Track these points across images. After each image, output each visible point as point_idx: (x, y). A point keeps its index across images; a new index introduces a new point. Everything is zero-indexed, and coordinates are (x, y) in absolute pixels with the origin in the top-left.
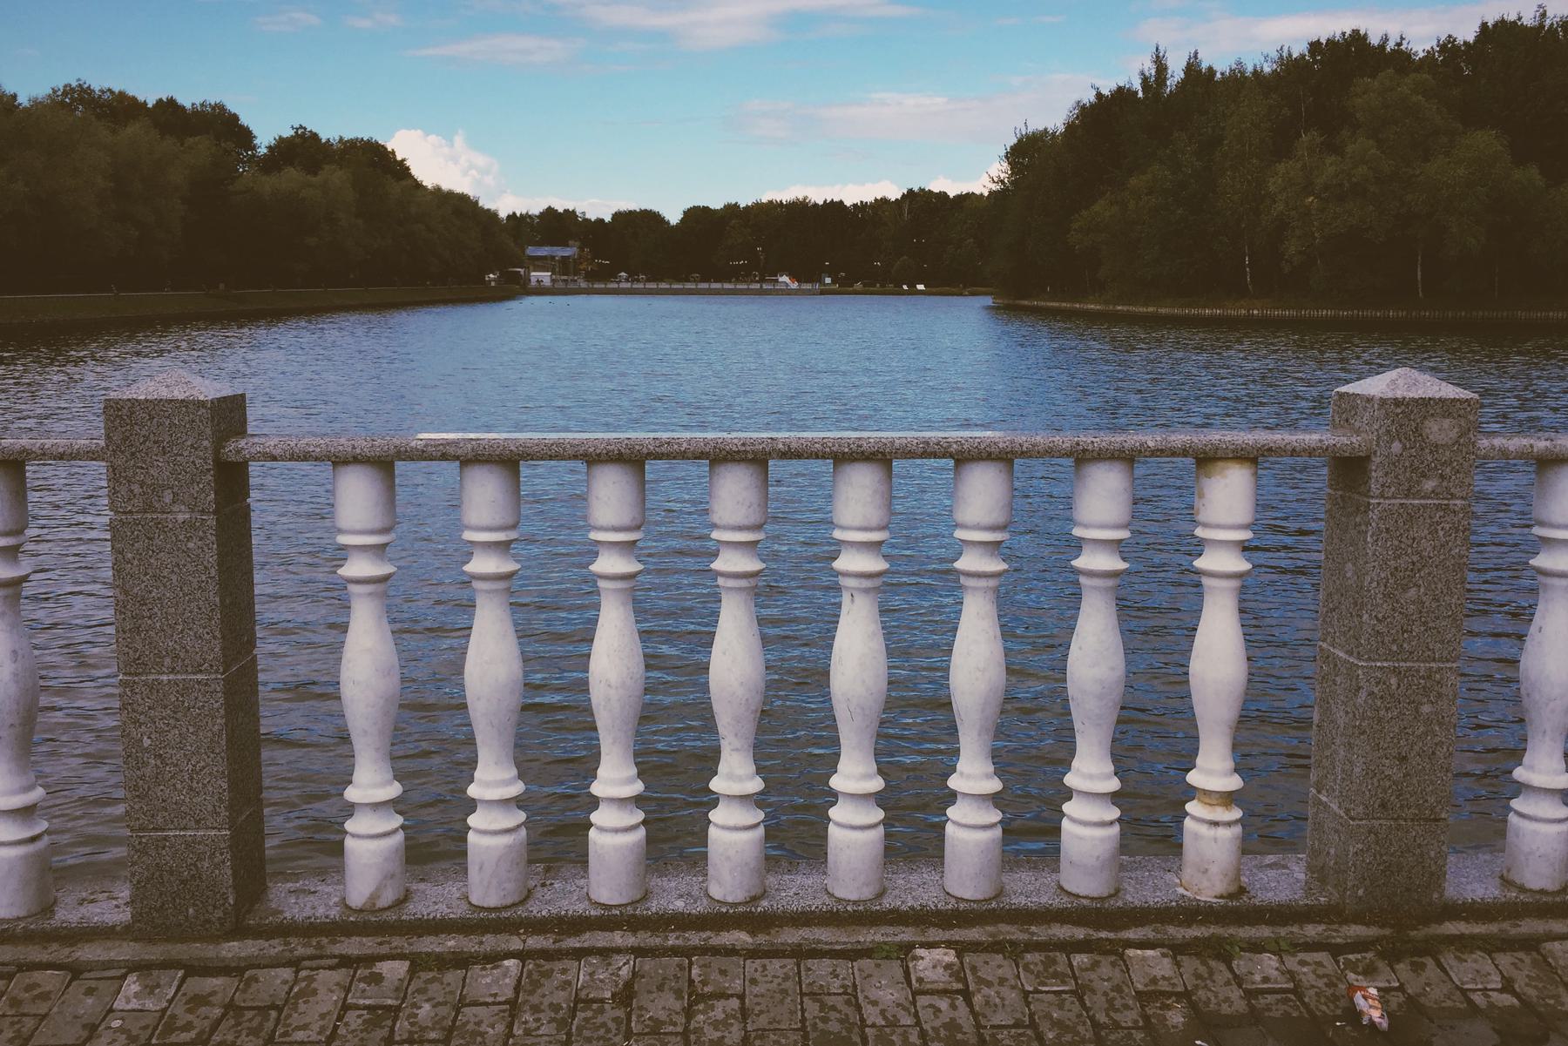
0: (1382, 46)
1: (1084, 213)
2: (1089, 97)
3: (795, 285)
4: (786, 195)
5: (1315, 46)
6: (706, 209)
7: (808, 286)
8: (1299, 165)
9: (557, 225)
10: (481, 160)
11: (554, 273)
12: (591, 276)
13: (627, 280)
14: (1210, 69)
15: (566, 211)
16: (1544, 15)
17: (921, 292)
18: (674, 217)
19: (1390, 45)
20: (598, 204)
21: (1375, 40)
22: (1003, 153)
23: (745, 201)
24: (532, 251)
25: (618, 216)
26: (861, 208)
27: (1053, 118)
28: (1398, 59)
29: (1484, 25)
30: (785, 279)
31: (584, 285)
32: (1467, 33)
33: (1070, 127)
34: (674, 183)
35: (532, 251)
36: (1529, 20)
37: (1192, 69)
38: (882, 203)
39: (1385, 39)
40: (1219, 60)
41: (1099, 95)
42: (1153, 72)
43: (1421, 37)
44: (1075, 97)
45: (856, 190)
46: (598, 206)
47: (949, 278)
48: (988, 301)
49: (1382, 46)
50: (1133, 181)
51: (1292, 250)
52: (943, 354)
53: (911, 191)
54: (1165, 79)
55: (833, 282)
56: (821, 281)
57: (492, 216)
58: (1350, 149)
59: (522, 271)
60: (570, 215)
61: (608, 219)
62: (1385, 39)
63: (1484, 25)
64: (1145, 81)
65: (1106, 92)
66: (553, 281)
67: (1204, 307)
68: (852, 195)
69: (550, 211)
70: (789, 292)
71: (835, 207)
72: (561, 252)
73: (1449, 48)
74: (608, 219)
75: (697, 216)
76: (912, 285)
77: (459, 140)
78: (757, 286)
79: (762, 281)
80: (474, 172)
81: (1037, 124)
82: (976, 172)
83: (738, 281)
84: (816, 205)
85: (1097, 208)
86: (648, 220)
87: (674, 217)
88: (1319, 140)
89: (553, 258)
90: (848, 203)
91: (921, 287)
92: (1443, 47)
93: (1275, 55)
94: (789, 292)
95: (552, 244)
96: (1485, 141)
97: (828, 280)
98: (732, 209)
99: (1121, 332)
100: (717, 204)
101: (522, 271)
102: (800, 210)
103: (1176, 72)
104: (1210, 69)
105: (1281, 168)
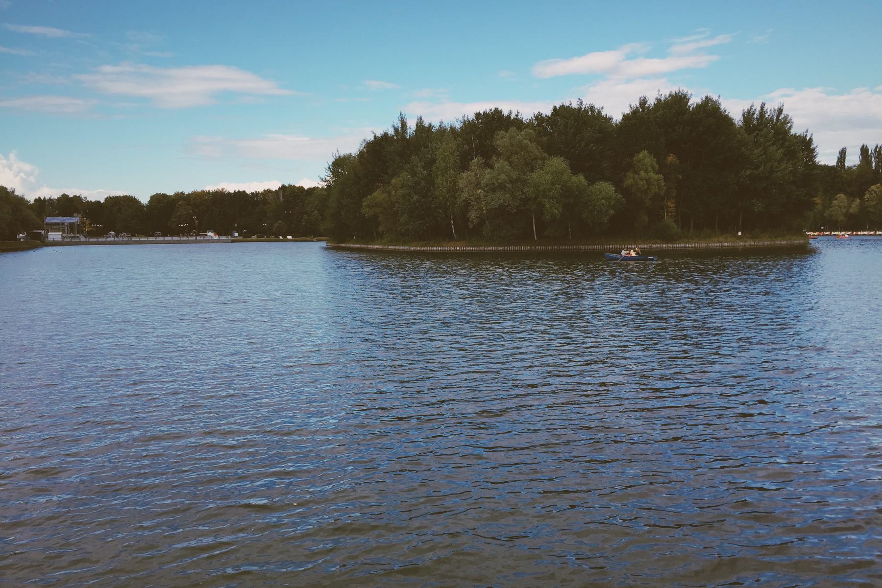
0: (509, 116)
1: (369, 197)
2: (371, 138)
3: (217, 237)
4: (211, 188)
5: (478, 115)
6: (164, 196)
7: (224, 238)
8: (473, 174)
9: (68, 205)
10: (27, 167)
11: (63, 232)
12: (91, 234)
13: (114, 237)
14: (430, 125)
15: (75, 196)
16: (581, 103)
17: (290, 240)
18: (144, 200)
19: (513, 116)
20: (95, 192)
21: (505, 113)
22: (327, 166)
23: (187, 191)
24: (49, 220)
25: (108, 199)
26: (255, 195)
27: (352, 147)
28: (516, 123)
29: (555, 108)
30: (210, 234)
31: (83, 239)
32: (547, 111)
33: (361, 153)
34: (145, 183)
35: (49, 220)
36: (575, 105)
37: (420, 126)
38: (268, 192)
39: (511, 113)
40: (433, 119)
41: (13, 192)
42: (400, 125)
43: (527, 113)
44: (685, 89)
45: (253, 185)
46: (96, 193)
47: (303, 231)
48: (324, 244)
49: (509, 116)
50: (393, 181)
51: (473, 216)
52: (302, 275)
53: (283, 186)
54: (406, 130)
55: (239, 235)
56: (232, 235)
57: (21, 200)
58: (497, 165)
59: (43, 232)
60: (77, 199)
61: (102, 201)
62: (511, 113)
63: (555, 108)
64: (396, 130)
65: (378, 135)
66: (63, 238)
67: (433, 246)
68: (252, 187)
69: (65, 197)
70: (214, 241)
71: (241, 195)
72: (68, 220)
73: (539, 118)
74: (102, 201)
75: (159, 200)
76: (285, 236)
77: (12, 156)
78: (194, 238)
79: (197, 235)
80: (22, 174)
81: (344, 152)
82: (313, 176)
83: (183, 235)
84: (229, 193)
85: (375, 194)
86: (129, 202)
87: (144, 200)
88: (481, 162)
89: (63, 224)
90: (248, 192)
91: (289, 237)
92: (536, 118)
93: (461, 119)
94: (214, 241)
95: (63, 216)
96: (558, 163)
97: (236, 234)
98: (180, 196)
99: (394, 263)
100: (170, 192)
101: (43, 232)
102: (220, 197)
103: (412, 126)
104: (430, 125)
105: (464, 175)
